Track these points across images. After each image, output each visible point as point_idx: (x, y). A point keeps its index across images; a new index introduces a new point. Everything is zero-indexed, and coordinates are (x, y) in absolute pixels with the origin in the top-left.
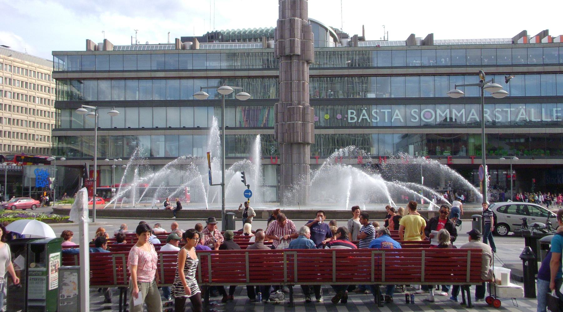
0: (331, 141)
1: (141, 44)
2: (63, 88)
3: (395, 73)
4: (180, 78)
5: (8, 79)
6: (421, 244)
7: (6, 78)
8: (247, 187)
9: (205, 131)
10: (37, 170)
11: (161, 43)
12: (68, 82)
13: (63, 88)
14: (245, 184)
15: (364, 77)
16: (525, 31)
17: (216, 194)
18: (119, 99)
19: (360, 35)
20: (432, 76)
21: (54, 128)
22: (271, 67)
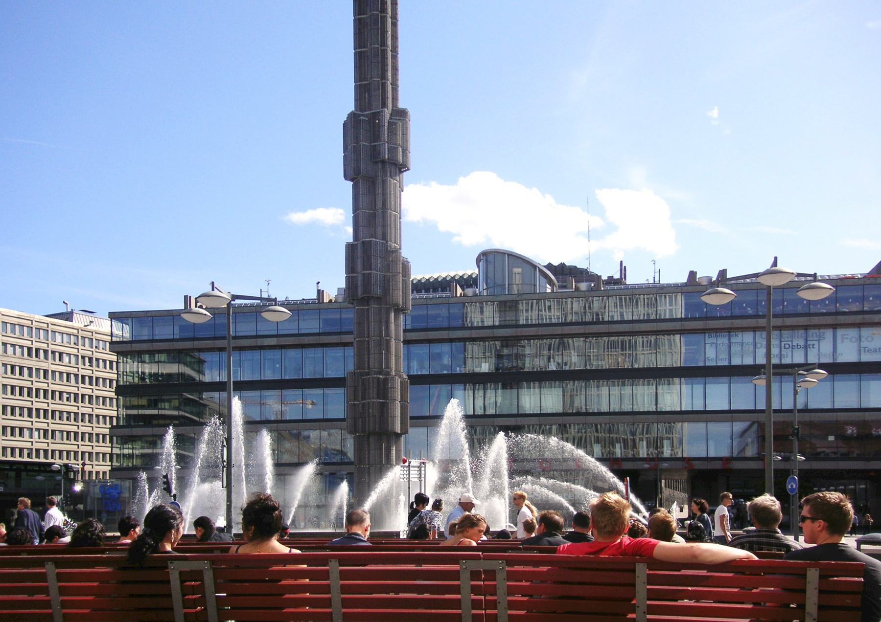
0: (599, 431)
1: (290, 299)
2: (199, 367)
3: (638, 330)
4: (430, 341)
5: (87, 359)
6: (524, 583)
7: (83, 357)
8: (172, 498)
9: (432, 420)
10: (841, 500)
11: (305, 298)
12: (147, 357)
13: (199, 367)
14: (170, 494)
15: (527, 340)
16: (690, 272)
17: (643, 526)
18: (212, 380)
19: (617, 276)
20: (700, 333)
21: (115, 424)
22: (601, 319)
